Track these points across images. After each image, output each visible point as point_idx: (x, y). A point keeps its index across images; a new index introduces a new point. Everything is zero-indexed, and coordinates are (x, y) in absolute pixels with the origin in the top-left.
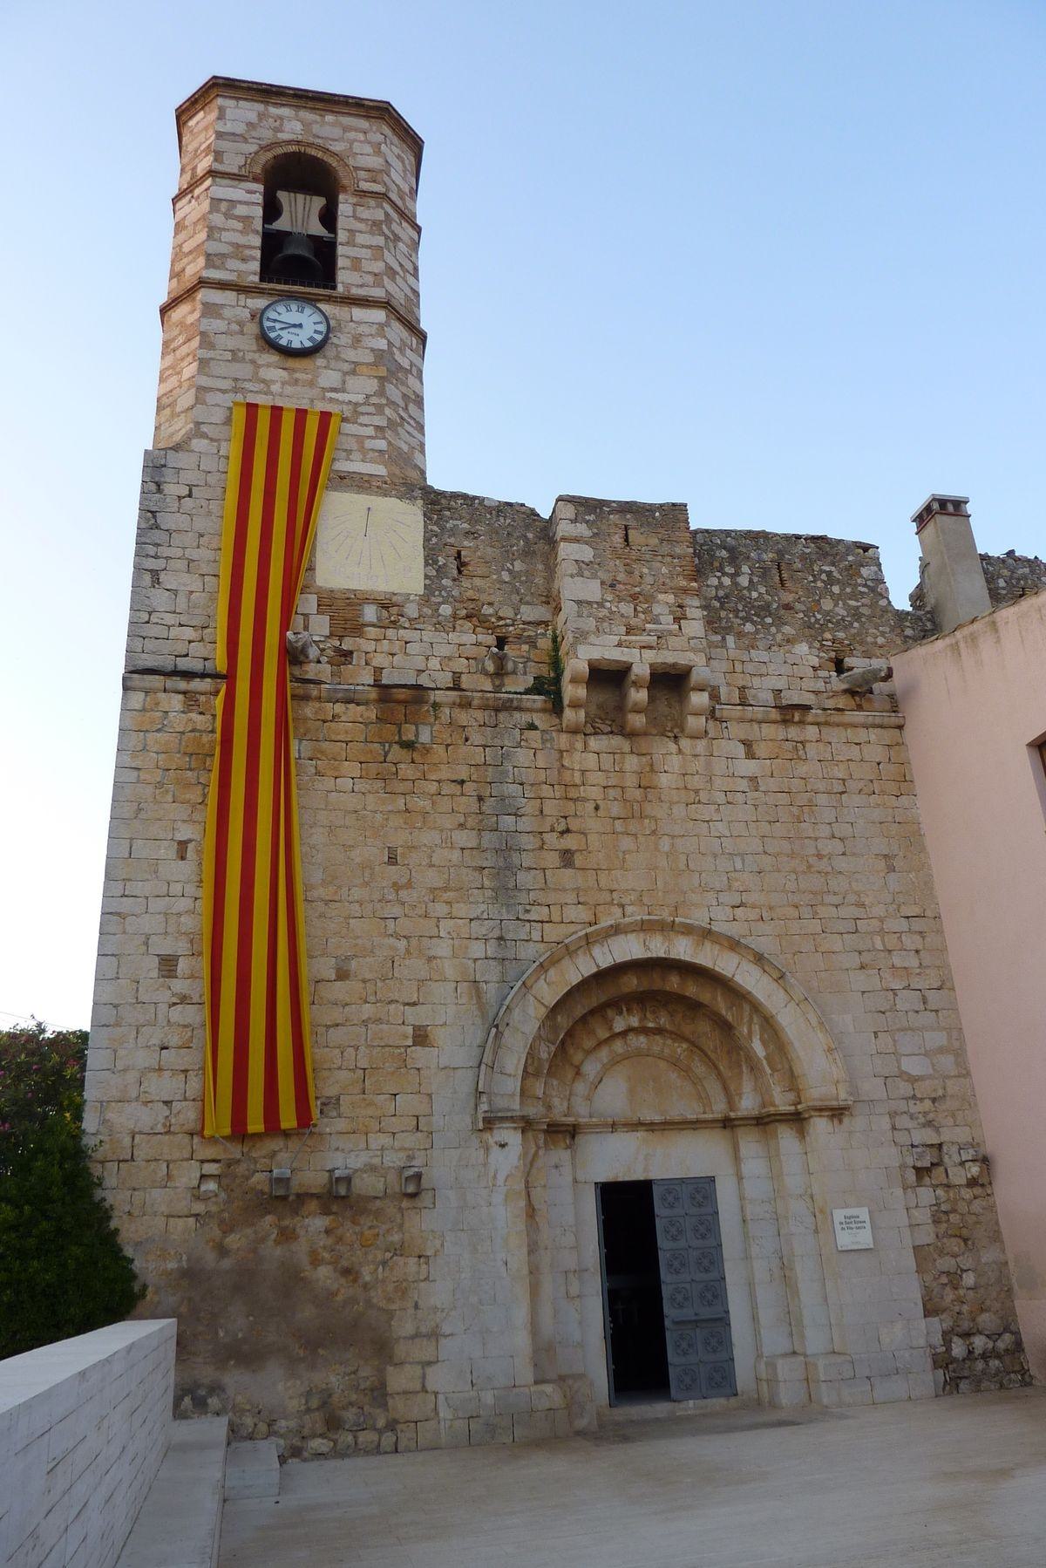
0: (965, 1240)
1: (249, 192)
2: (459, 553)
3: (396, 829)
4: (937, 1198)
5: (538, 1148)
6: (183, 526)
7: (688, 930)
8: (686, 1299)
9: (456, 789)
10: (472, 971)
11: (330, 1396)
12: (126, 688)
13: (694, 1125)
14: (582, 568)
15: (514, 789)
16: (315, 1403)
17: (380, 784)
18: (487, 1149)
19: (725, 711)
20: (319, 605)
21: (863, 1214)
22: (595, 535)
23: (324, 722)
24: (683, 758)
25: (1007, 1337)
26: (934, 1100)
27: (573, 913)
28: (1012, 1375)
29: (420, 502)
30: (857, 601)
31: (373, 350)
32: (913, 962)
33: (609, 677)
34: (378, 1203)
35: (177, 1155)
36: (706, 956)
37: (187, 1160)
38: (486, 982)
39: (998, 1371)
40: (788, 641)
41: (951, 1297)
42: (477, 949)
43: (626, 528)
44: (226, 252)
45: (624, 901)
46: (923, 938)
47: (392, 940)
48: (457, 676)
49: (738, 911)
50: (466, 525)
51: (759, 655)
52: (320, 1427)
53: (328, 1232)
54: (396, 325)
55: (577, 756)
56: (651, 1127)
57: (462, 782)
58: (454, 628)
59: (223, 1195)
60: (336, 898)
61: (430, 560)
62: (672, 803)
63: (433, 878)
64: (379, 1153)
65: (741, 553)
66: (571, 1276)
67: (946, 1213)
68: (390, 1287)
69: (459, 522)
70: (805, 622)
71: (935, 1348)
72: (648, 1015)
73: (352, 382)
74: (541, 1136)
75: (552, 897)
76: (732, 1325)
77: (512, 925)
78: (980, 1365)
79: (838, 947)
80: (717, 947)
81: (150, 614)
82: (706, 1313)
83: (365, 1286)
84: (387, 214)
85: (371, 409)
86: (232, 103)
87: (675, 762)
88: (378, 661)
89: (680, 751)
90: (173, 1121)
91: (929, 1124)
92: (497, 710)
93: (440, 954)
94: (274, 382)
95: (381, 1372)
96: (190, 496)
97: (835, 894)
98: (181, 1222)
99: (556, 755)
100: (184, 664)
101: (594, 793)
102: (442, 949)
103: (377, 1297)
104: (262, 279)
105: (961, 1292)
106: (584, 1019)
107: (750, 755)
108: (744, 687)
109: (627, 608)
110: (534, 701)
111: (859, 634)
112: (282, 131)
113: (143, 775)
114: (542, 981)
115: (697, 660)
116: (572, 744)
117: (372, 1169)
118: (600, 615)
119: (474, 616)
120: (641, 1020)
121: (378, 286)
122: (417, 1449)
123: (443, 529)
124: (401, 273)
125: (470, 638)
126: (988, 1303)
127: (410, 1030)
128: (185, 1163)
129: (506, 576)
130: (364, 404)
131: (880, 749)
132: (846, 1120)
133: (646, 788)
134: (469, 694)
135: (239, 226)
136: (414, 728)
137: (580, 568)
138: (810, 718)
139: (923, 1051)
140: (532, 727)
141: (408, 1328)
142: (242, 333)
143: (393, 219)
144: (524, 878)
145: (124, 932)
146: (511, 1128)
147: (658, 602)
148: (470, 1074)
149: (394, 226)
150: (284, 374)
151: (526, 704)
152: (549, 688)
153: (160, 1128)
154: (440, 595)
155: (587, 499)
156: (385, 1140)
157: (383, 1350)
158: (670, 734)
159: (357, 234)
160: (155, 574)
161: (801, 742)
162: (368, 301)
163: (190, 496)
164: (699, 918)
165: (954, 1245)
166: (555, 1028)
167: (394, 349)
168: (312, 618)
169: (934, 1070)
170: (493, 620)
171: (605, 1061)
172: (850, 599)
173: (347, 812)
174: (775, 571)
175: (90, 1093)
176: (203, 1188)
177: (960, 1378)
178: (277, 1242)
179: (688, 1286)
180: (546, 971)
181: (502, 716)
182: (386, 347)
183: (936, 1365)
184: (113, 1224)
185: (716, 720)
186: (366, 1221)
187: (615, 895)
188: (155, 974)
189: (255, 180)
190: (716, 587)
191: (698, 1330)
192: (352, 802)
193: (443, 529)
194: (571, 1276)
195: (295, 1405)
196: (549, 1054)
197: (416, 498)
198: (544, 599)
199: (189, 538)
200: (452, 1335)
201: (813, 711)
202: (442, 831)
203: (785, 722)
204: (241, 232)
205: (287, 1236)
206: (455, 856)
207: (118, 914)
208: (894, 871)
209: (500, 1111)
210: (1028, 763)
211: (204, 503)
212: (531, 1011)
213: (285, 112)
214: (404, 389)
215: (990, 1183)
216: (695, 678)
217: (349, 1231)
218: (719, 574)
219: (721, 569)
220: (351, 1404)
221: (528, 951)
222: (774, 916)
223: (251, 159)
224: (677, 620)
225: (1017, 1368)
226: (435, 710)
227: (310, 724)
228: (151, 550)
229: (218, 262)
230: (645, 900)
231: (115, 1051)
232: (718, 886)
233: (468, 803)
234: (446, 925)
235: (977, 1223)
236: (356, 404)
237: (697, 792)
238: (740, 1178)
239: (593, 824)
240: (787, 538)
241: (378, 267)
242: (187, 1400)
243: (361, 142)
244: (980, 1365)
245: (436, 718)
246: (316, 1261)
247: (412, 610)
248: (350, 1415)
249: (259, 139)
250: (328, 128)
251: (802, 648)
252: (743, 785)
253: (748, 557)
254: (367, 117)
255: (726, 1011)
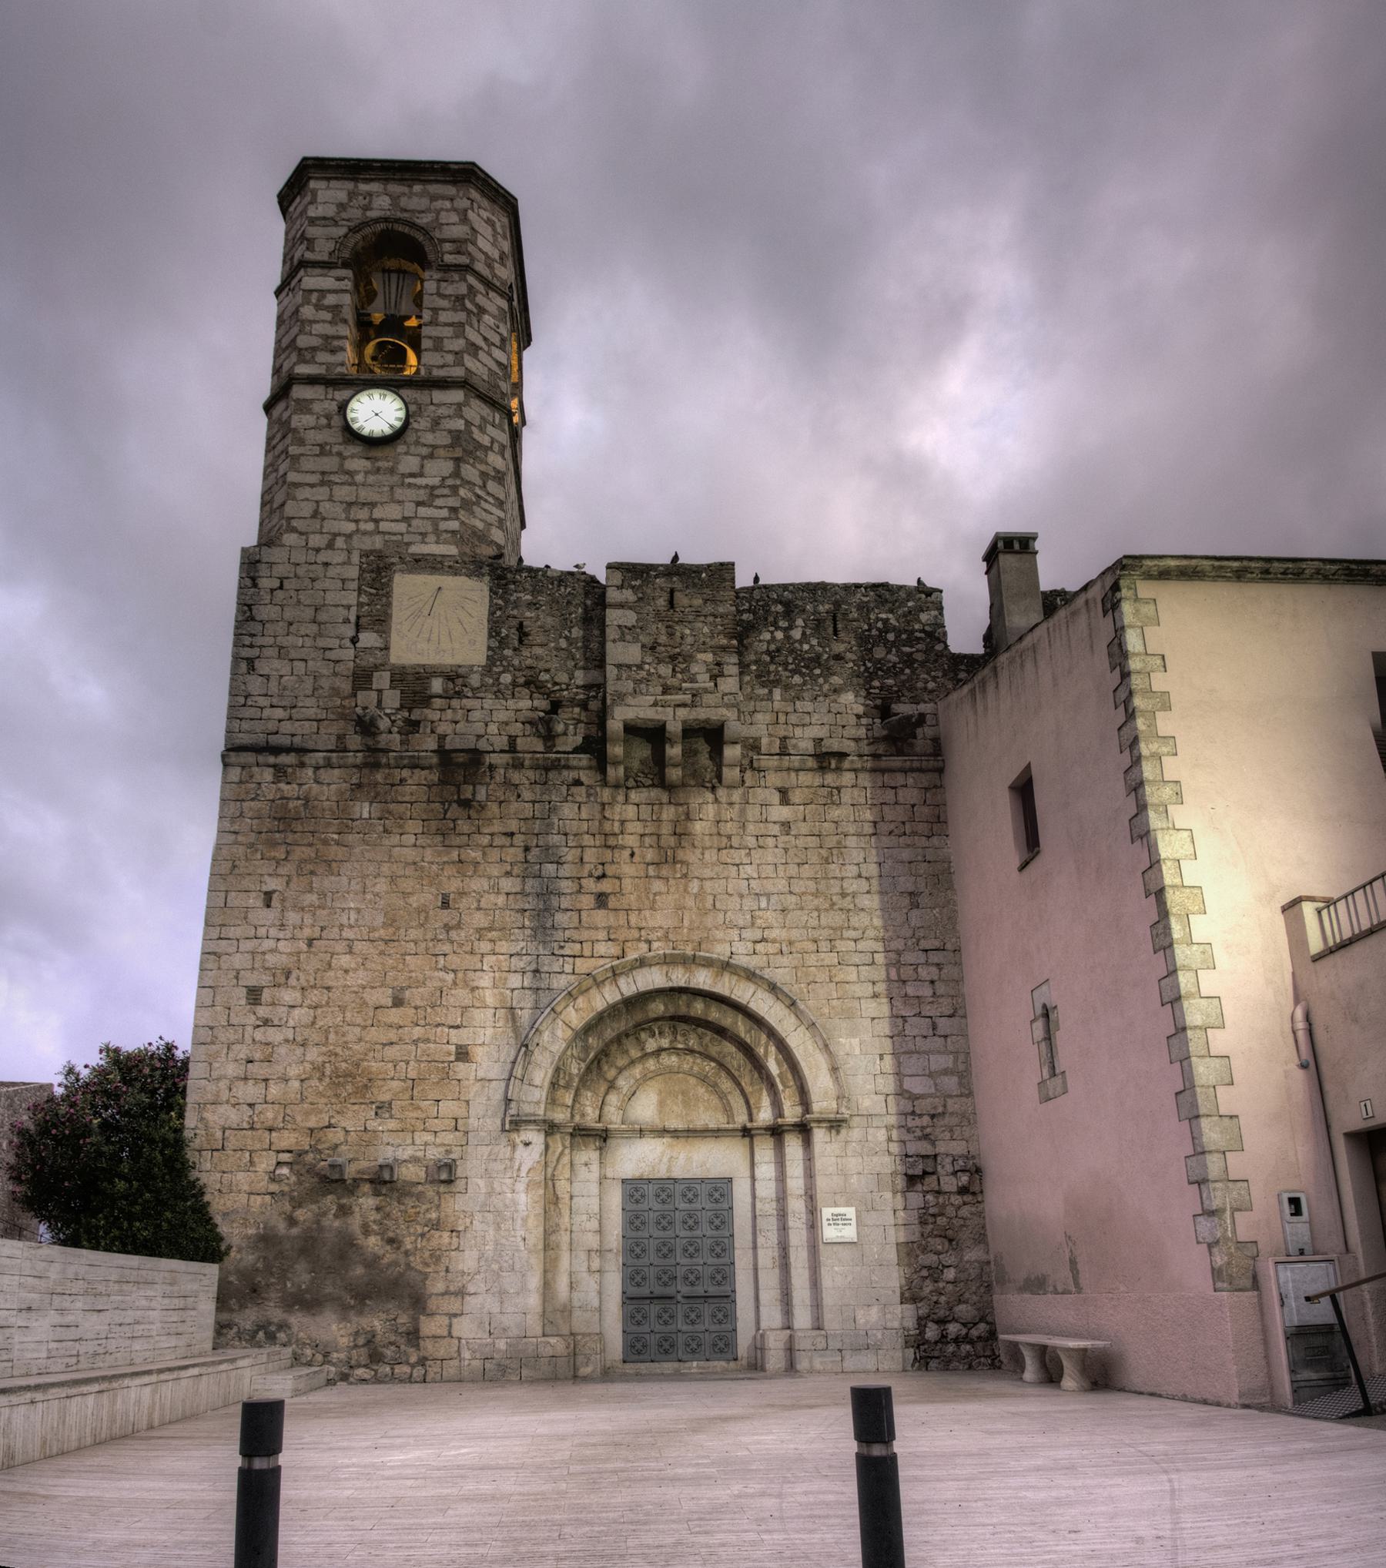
0: (951, 1241)
1: (339, 279)
2: (521, 625)
3: (449, 878)
4: (925, 1202)
5: (565, 1147)
6: (273, 616)
7: (708, 963)
8: (698, 1278)
9: (506, 841)
10: (509, 999)
11: (374, 1336)
12: (226, 765)
13: (717, 1133)
14: (626, 632)
15: (556, 839)
16: (361, 1341)
17: (439, 838)
18: (514, 1147)
19: (765, 762)
20: (391, 681)
21: (850, 1212)
22: (640, 599)
23: (393, 785)
24: (719, 808)
25: (982, 1326)
26: (933, 1117)
27: (602, 948)
28: (982, 1359)
29: (487, 578)
30: (912, 647)
31: (450, 432)
32: (926, 991)
33: (654, 735)
34: (420, 1188)
35: (258, 1146)
36: (725, 986)
37: (265, 1150)
38: (521, 1009)
39: (968, 1355)
40: (835, 691)
41: (930, 1288)
42: (515, 981)
43: (672, 592)
44: (316, 345)
45: (650, 937)
46: (940, 970)
47: (441, 974)
48: (512, 740)
49: (759, 947)
50: (529, 597)
51: (804, 705)
52: (364, 1360)
53: (378, 1209)
54: (476, 403)
55: (618, 808)
56: (675, 1134)
57: (512, 834)
58: (513, 694)
59: (293, 1179)
60: (396, 938)
61: (494, 632)
62: (704, 848)
63: (480, 920)
64: (422, 1148)
65: (796, 606)
66: (593, 1254)
67: (934, 1215)
68: (427, 1254)
69: (522, 595)
70: (854, 671)
71: (908, 1330)
72: (679, 1038)
73: (431, 467)
74: (568, 1138)
75: (585, 935)
76: (202, 924)
77: (546, 960)
78: (951, 1348)
79: (853, 977)
80: (735, 978)
81: (246, 697)
82: (713, 1290)
83: (407, 1253)
84: (471, 287)
85: (446, 491)
86: (322, 184)
87: (710, 811)
88: (444, 728)
89: (716, 801)
90: (256, 1119)
91: (926, 1137)
92: (547, 769)
93: (483, 985)
94: (357, 472)
95: (415, 1320)
96: (281, 587)
97: (855, 929)
98: (259, 1199)
99: (598, 807)
100: (274, 740)
101: (631, 841)
102: (485, 981)
103: (416, 1261)
104: (1353, 1137)
105: (941, 1285)
106: (618, 1040)
107: (785, 801)
108: (785, 738)
109: (665, 670)
110: (580, 759)
111: (908, 680)
112: (371, 209)
113: (240, 838)
114: (570, 1008)
115: (730, 715)
116: (614, 798)
117: (415, 1160)
118: (638, 677)
119: (532, 684)
120: (671, 1042)
121: (458, 365)
122: (442, 1381)
123: (507, 601)
124: (486, 348)
125: (525, 704)
126: (967, 1295)
127: (453, 1048)
128: (264, 1153)
129: (563, 644)
130: (440, 487)
131: (916, 791)
132: (843, 1132)
133: (680, 835)
134: (521, 755)
135: (328, 316)
136: (471, 787)
137: (623, 634)
138: (846, 764)
139: (927, 1072)
140: (578, 783)
141: (440, 1287)
142: (329, 426)
143: (478, 291)
144: (561, 918)
145: (219, 968)
146: (916, 1503)
147: (697, 661)
148: (503, 1084)
149: (480, 299)
150: (367, 464)
151: (575, 763)
152: (595, 747)
153: (245, 1125)
154: (502, 665)
155: (634, 565)
156: (428, 1137)
157: (418, 1303)
158: (708, 785)
159: (507, 748)
160: (250, 662)
161: (837, 788)
162: (446, 382)
163: (281, 587)
164: (720, 951)
165: (938, 1244)
166: (586, 1049)
167: (473, 428)
168: (385, 693)
169: (936, 1090)
170: (549, 685)
171: (638, 1077)
172: (904, 646)
173: (407, 864)
174: (829, 623)
175: (192, 1098)
176: (278, 1172)
177: (931, 1358)
178: (336, 1216)
179: (700, 1268)
180: (575, 999)
181: (551, 775)
182: (462, 428)
183: (907, 1344)
184: (207, 1198)
185: (754, 769)
186: (410, 1202)
187: (643, 933)
188: (243, 1002)
189: (345, 265)
190: (768, 642)
191: (652, 1306)
192: (410, 854)
193: (507, 601)
194: (593, 1254)
195: (344, 1341)
196: (579, 1070)
197: (483, 575)
198: (597, 663)
199: (280, 628)
200: (475, 1294)
201: (850, 758)
202: (490, 878)
203: (823, 769)
204: (330, 322)
205: (344, 1211)
206: (501, 900)
207: (215, 954)
208: (918, 907)
209: (526, 1115)
210: (810, 1084)
211: (293, 593)
212: (559, 1033)
213: (374, 187)
214: (483, 467)
215: (982, 1192)
216: (728, 733)
217: (395, 1210)
218: (772, 629)
219: (775, 624)
220: (391, 1343)
221: (561, 982)
222: (794, 950)
223: (341, 242)
224: (714, 678)
225: (988, 1353)
226: (491, 771)
227: (380, 789)
228: (247, 640)
229: (308, 356)
230: (671, 936)
231: (211, 1064)
232: (741, 923)
233: (514, 854)
234: (489, 960)
235: (962, 1226)
236: (433, 488)
237: (729, 837)
238: (753, 1178)
239: (628, 869)
240: (846, 587)
241: (459, 344)
242: (261, 1334)
243: (447, 210)
244: (951, 1348)
245: (492, 778)
246: (366, 1231)
247: (475, 680)
248: (389, 1352)
249: (348, 220)
250: (415, 199)
251: (848, 697)
252: (775, 829)
253: (804, 610)
254: (454, 183)
255: (746, 1033)
